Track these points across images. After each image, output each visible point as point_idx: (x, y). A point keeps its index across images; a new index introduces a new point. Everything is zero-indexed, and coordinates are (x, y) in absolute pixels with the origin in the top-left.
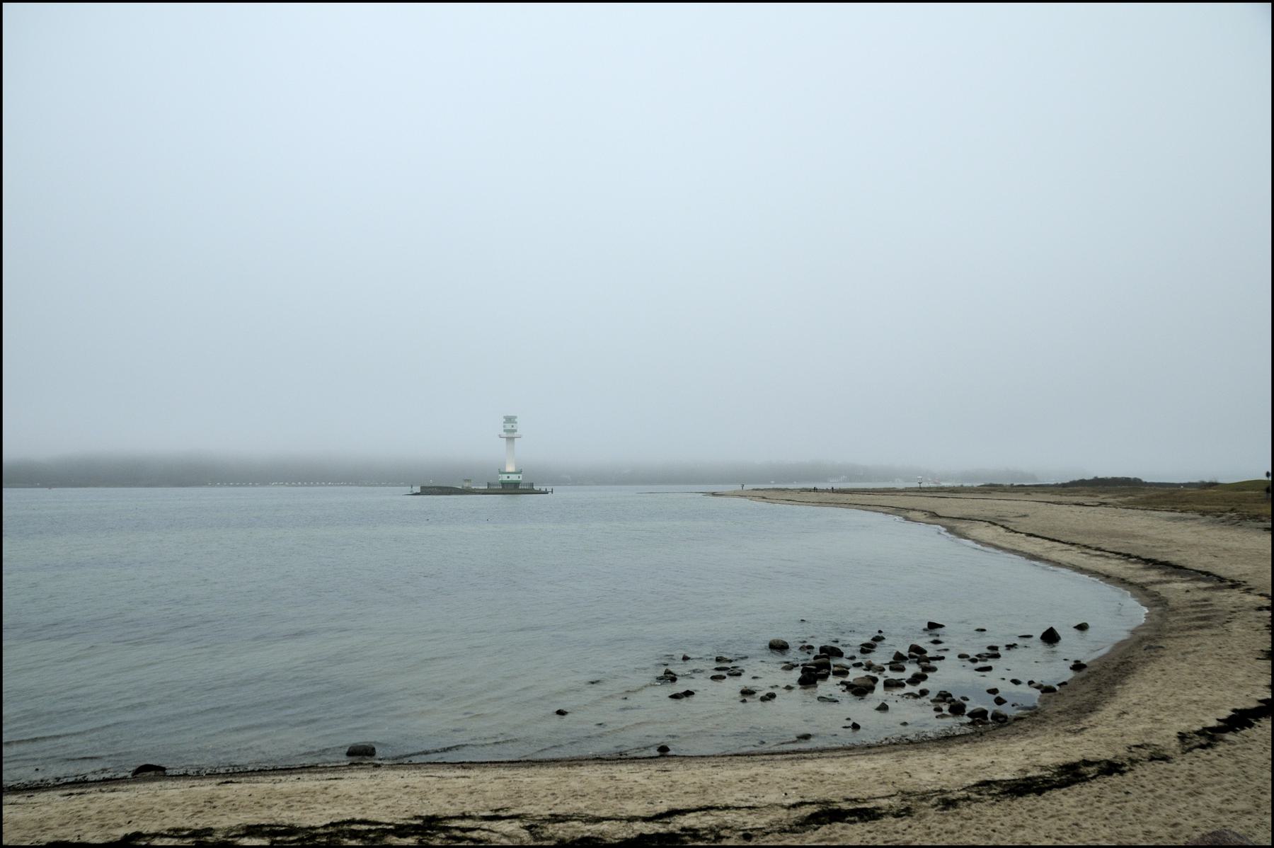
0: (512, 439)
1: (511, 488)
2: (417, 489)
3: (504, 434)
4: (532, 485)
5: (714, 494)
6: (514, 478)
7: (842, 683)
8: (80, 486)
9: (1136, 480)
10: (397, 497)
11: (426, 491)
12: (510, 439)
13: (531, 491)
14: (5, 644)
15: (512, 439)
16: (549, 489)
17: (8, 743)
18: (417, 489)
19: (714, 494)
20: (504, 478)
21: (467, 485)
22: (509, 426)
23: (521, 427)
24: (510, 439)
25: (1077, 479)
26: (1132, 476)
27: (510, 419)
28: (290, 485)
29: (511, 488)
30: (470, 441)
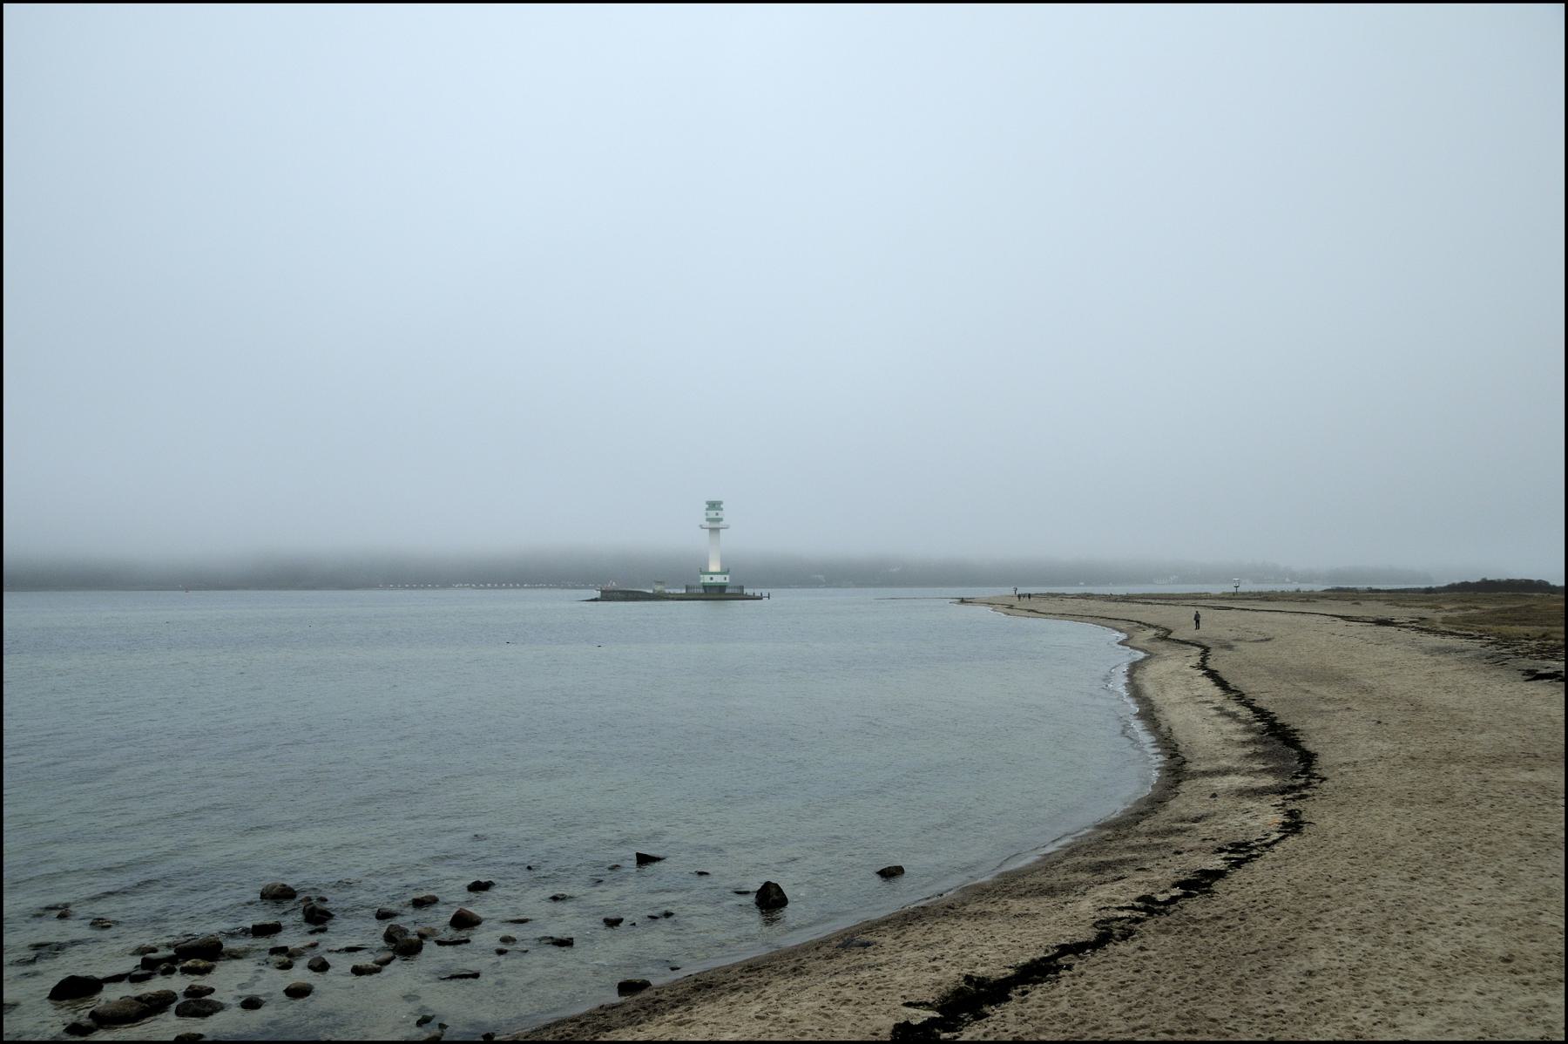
0: (717, 530)
1: (716, 593)
2: (598, 594)
3: (707, 524)
4: (742, 588)
5: (963, 601)
6: (719, 579)
7: (274, 951)
8: (314, 588)
9: (1540, 582)
10: (567, 604)
11: (608, 596)
12: (714, 530)
13: (741, 597)
14: (6, 826)
15: (717, 530)
16: (765, 592)
17: (1530, 759)
18: (598, 594)
19: (963, 601)
20: (706, 579)
21: (659, 588)
22: (712, 514)
23: (727, 514)
24: (714, 530)
25: (1457, 581)
26: (1535, 578)
27: (714, 505)
28: (478, 587)
29: (716, 593)
30: (662, 529)
